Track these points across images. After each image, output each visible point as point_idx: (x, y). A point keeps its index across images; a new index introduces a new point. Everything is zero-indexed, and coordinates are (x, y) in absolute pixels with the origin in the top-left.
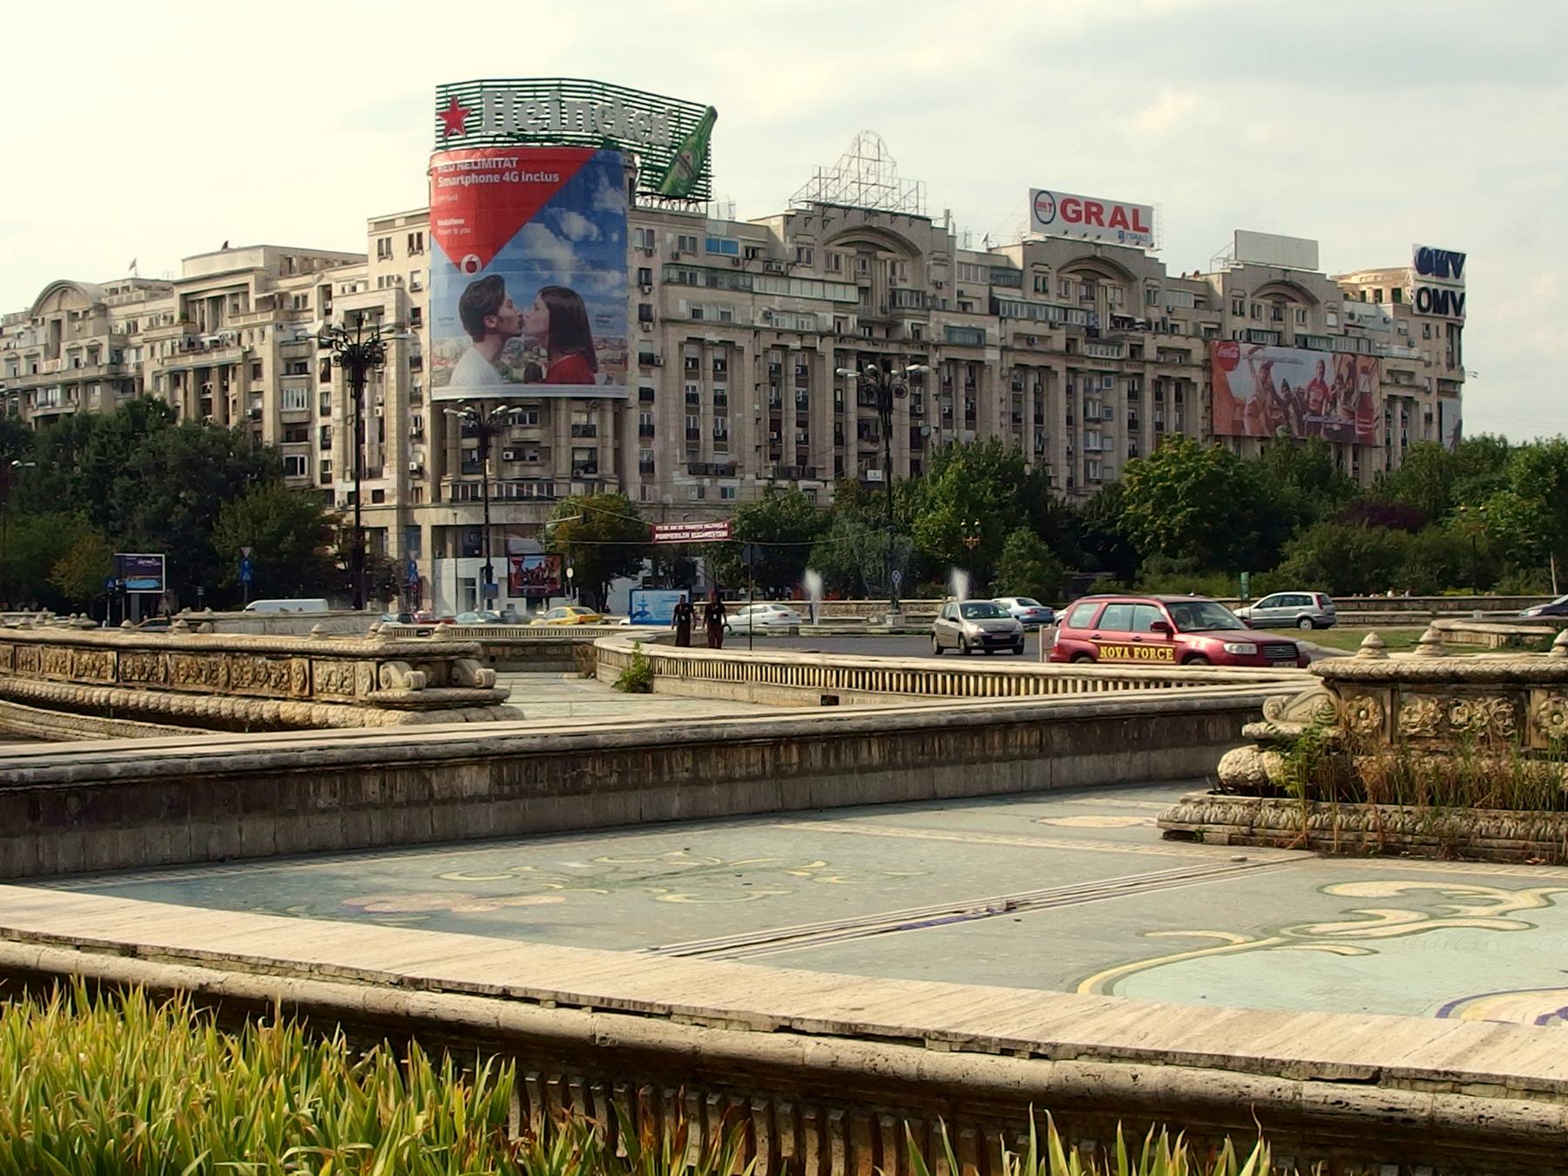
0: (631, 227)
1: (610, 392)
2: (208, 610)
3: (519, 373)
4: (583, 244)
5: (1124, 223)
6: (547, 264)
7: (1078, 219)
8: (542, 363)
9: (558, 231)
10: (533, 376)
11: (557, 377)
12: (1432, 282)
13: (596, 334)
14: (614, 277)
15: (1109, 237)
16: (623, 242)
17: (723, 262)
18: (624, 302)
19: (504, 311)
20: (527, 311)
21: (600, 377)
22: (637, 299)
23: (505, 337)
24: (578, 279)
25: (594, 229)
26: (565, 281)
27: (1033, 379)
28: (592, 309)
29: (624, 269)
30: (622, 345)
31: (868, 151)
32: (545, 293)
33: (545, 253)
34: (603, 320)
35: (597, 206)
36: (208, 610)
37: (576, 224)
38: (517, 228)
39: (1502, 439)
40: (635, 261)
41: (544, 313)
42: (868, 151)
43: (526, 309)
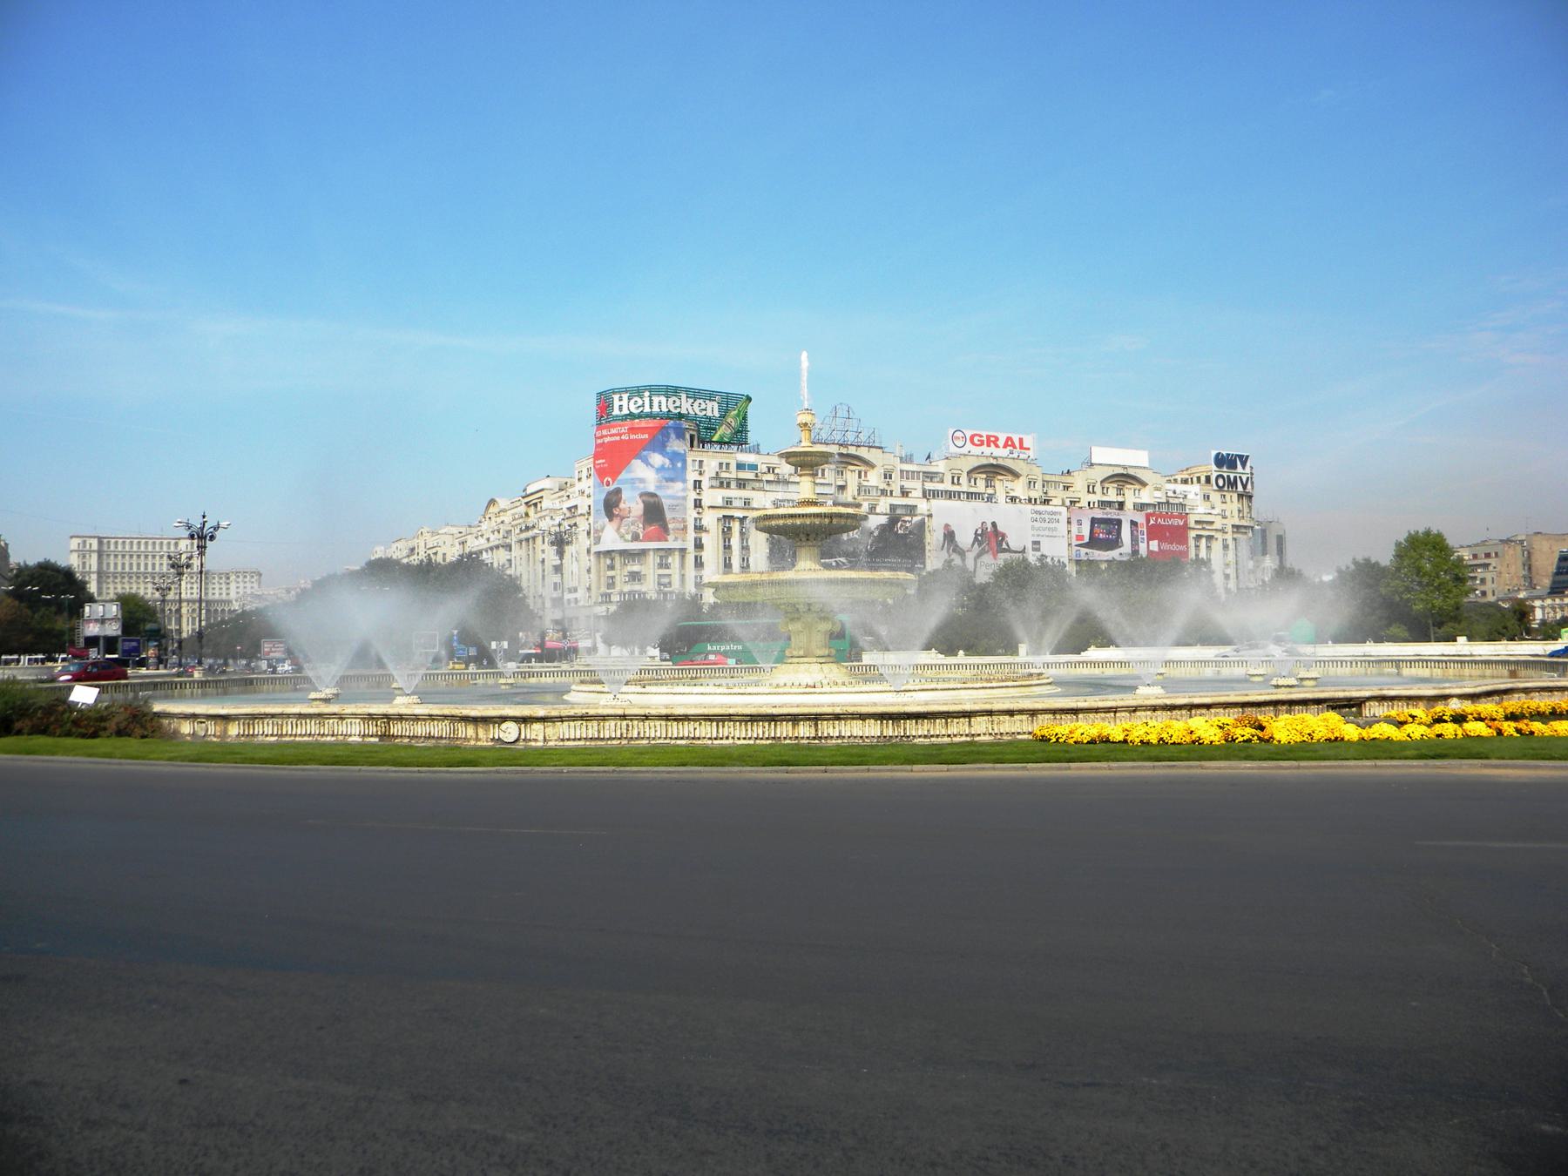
0: (689, 460)
1: (678, 545)
2: (1462, 640)
3: (629, 537)
4: (661, 469)
5: (1013, 445)
6: (642, 481)
7: (982, 443)
8: (640, 531)
9: (648, 464)
10: (636, 538)
11: (648, 538)
12: (1225, 471)
13: (668, 515)
14: (679, 485)
15: (1002, 452)
16: (684, 467)
17: (749, 475)
18: (685, 498)
19: (622, 505)
20: (633, 505)
21: (671, 538)
22: (693, 495)
23: (622, 518)
24: (658, 488)
25: (667, 461)
26: (652, 489)
27: (1204, 541)
28: (666, 503)
29: (684, 481)
30: (684, 520)
31: (842, 413)
32: (641, 495)
33: (641, 475)
34: (673, 508)
35: (668, 449)
36: (1462, 640)
37: (657, 459)
38: (629, 462)
39: (1355, 562)
40: (692, 476)
41: (641, 506)
42: (842, 413)
43: (632, 504)
